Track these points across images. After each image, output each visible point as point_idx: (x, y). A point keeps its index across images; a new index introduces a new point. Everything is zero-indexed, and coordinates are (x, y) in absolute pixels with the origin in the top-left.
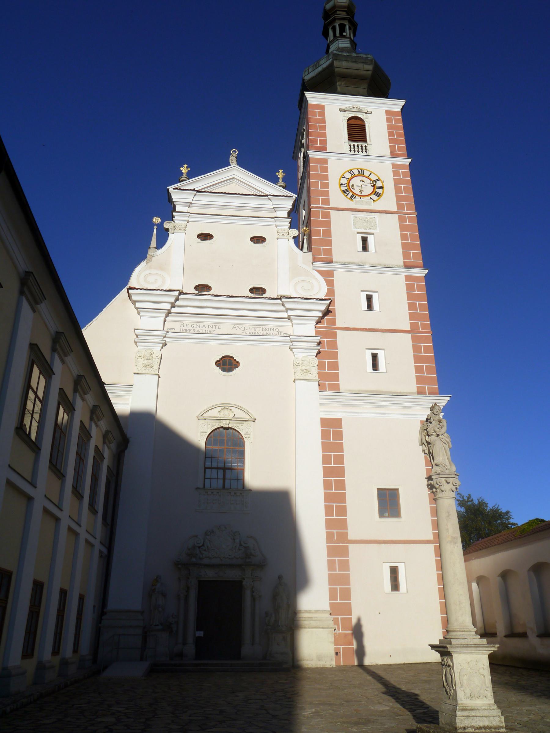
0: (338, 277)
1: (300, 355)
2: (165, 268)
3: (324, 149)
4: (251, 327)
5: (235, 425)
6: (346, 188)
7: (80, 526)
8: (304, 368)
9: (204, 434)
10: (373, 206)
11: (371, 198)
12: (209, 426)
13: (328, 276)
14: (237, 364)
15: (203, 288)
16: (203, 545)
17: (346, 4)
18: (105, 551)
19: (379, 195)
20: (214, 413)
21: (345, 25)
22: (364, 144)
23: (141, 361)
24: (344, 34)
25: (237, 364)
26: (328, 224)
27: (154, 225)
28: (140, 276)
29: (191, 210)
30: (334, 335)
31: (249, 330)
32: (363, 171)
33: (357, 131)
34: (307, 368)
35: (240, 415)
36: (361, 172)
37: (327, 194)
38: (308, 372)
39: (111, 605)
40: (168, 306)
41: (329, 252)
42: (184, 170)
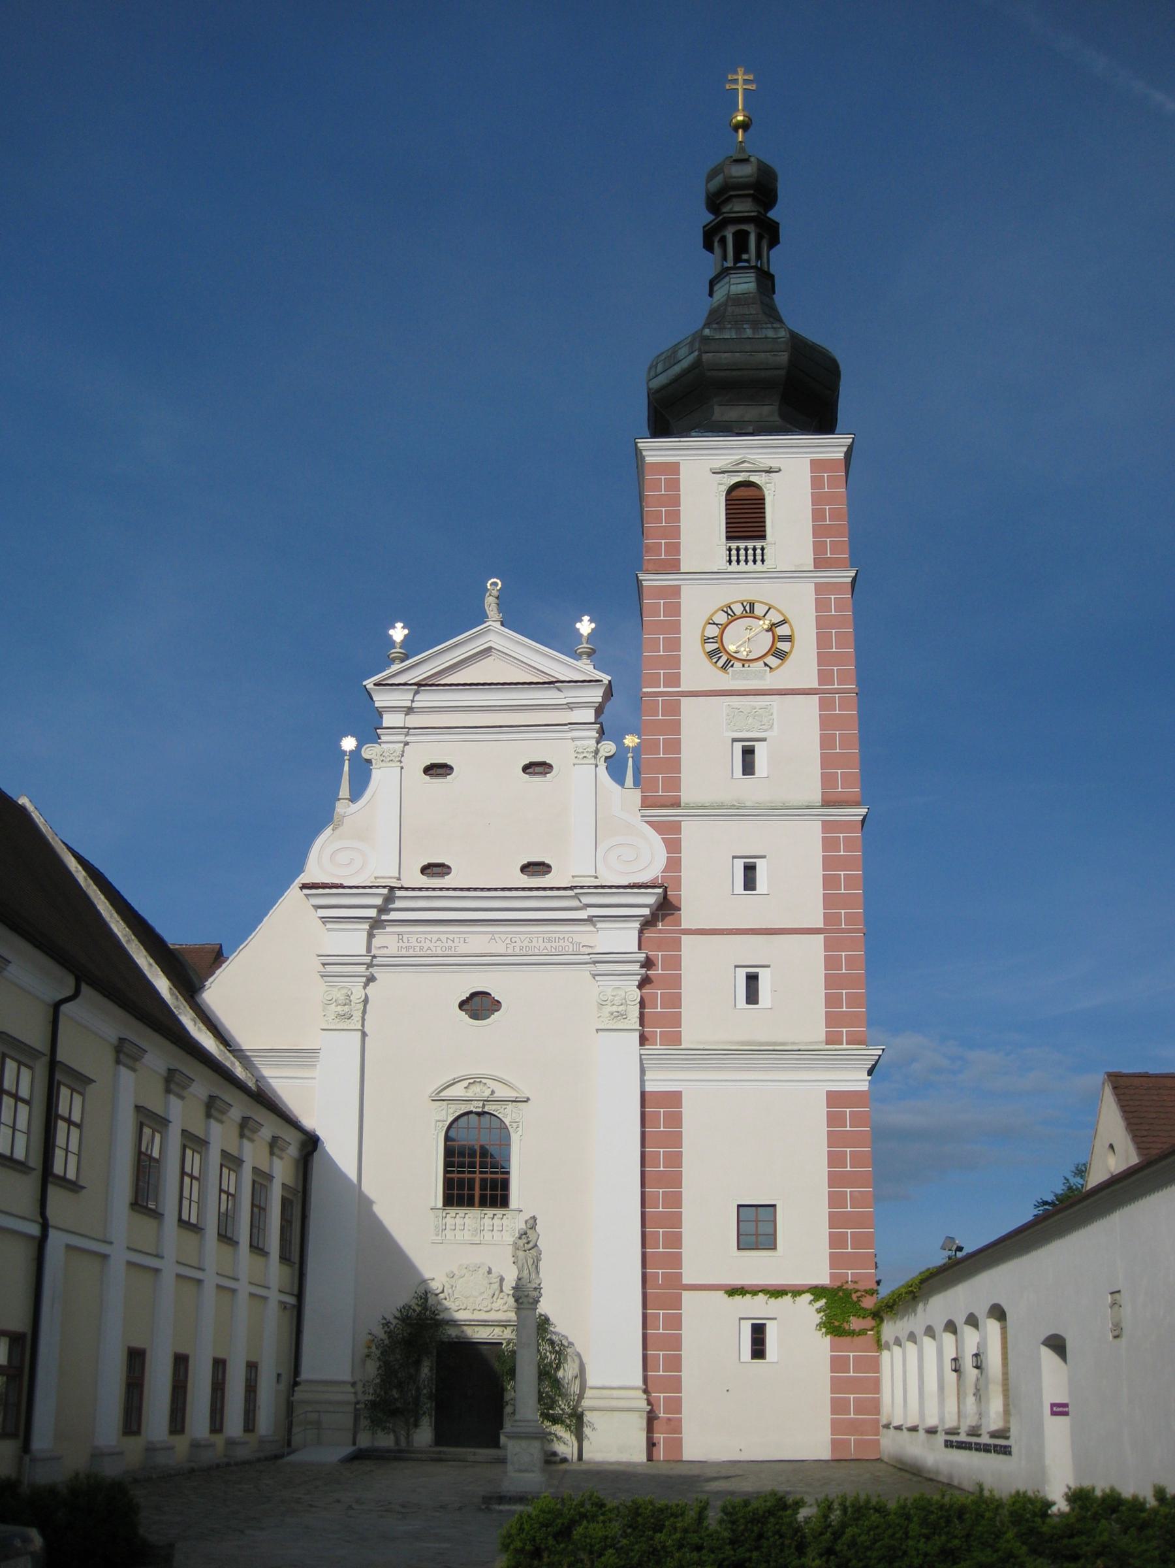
0: (691, 832)
1: (609, 986)
2: (361, 844)
3: (673, 566)
4: (523, 937)
5: (494, 1107)
6: (715, 646)
7: (269, 1288)
8: (615, 1008)
9: (440, 1124)
10: (770, 681)
11: (766, 665)
12: (451, 1111)
13: (670, 833)
14: (496, 1005)
15: (433, 869)
16: (443, 1292)
17: (753, 180)
18: (291, 1300)
19: (782, 655)
20: (458, 1091)
21: (747, 233)
22: (758, 544)
23: (333, 1007)
24: (745, 257)
25: (496, 1005)
26: (675, 727)
27: (344, 753)
28: (325, 859)
29: (413, 720)
30: (677, 945)
31: (519, 944)
32: (752, 605)
33: (745, 515)
34: (620, 1008)
35: (502, 1092)
36: (748, 608)
37: (675, 662)
38: (623, 1016)
39: (305, 1375)
40: (372, 913)
41: (674, 784)
42: (398, 633)
